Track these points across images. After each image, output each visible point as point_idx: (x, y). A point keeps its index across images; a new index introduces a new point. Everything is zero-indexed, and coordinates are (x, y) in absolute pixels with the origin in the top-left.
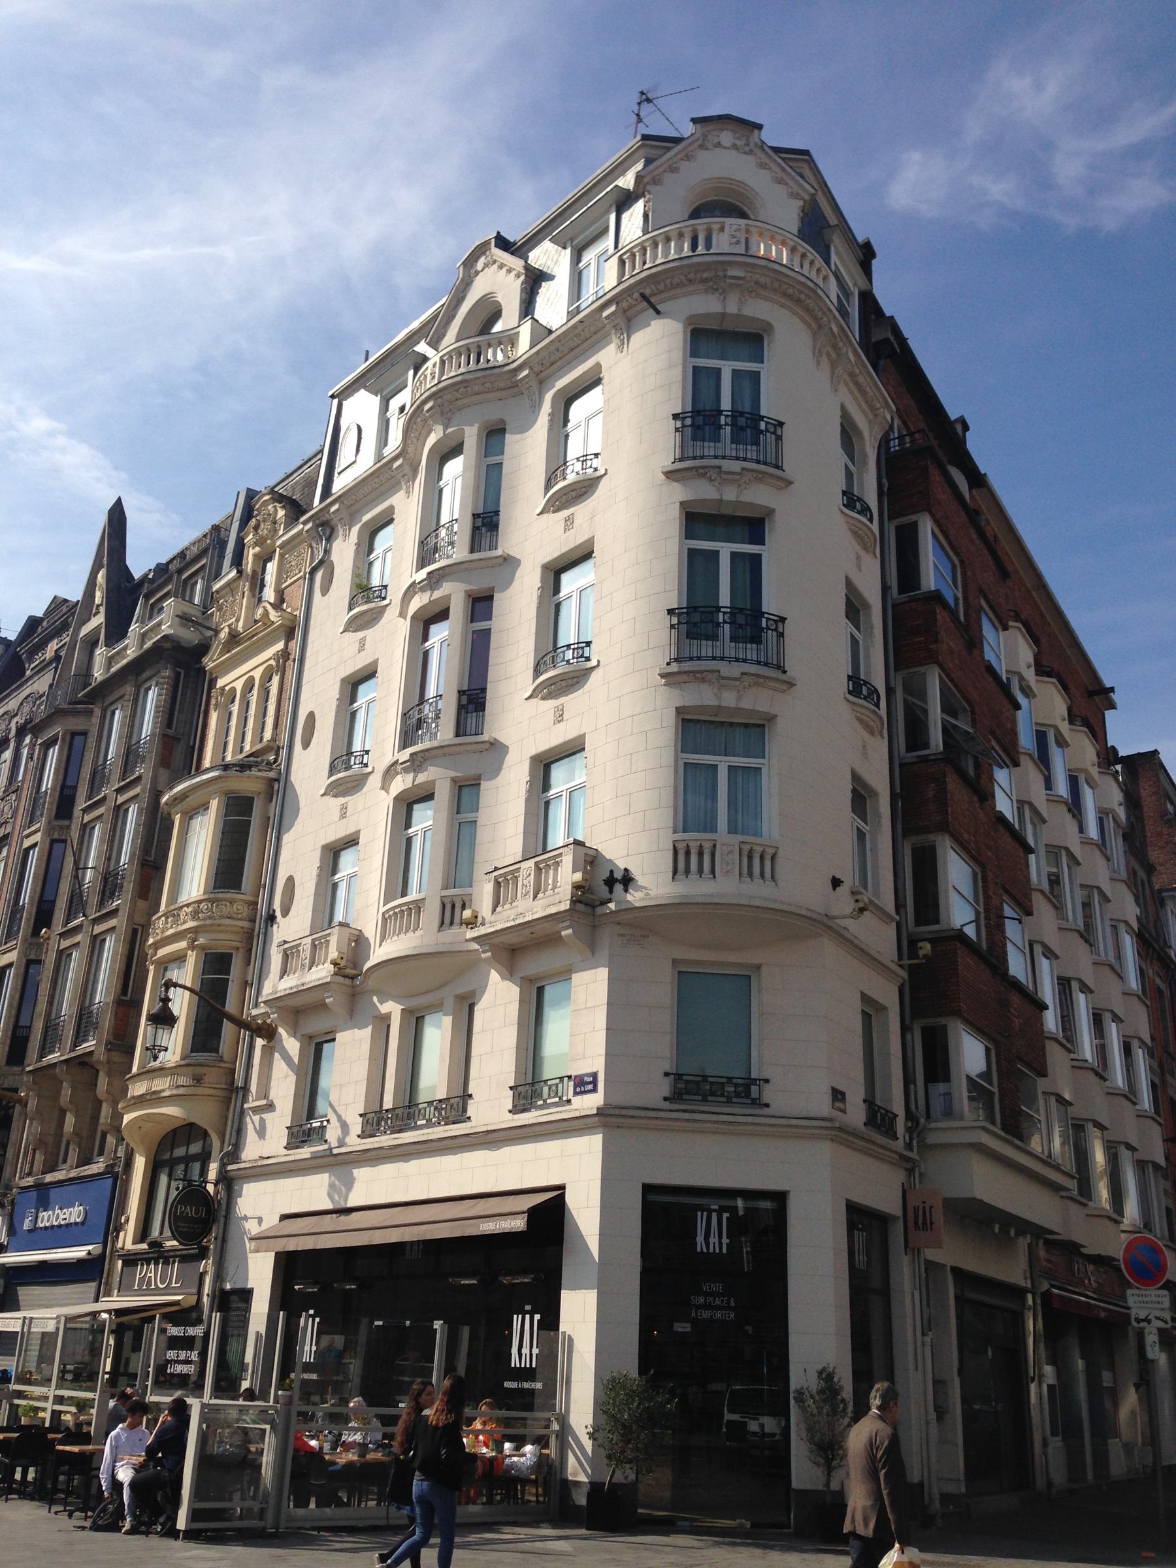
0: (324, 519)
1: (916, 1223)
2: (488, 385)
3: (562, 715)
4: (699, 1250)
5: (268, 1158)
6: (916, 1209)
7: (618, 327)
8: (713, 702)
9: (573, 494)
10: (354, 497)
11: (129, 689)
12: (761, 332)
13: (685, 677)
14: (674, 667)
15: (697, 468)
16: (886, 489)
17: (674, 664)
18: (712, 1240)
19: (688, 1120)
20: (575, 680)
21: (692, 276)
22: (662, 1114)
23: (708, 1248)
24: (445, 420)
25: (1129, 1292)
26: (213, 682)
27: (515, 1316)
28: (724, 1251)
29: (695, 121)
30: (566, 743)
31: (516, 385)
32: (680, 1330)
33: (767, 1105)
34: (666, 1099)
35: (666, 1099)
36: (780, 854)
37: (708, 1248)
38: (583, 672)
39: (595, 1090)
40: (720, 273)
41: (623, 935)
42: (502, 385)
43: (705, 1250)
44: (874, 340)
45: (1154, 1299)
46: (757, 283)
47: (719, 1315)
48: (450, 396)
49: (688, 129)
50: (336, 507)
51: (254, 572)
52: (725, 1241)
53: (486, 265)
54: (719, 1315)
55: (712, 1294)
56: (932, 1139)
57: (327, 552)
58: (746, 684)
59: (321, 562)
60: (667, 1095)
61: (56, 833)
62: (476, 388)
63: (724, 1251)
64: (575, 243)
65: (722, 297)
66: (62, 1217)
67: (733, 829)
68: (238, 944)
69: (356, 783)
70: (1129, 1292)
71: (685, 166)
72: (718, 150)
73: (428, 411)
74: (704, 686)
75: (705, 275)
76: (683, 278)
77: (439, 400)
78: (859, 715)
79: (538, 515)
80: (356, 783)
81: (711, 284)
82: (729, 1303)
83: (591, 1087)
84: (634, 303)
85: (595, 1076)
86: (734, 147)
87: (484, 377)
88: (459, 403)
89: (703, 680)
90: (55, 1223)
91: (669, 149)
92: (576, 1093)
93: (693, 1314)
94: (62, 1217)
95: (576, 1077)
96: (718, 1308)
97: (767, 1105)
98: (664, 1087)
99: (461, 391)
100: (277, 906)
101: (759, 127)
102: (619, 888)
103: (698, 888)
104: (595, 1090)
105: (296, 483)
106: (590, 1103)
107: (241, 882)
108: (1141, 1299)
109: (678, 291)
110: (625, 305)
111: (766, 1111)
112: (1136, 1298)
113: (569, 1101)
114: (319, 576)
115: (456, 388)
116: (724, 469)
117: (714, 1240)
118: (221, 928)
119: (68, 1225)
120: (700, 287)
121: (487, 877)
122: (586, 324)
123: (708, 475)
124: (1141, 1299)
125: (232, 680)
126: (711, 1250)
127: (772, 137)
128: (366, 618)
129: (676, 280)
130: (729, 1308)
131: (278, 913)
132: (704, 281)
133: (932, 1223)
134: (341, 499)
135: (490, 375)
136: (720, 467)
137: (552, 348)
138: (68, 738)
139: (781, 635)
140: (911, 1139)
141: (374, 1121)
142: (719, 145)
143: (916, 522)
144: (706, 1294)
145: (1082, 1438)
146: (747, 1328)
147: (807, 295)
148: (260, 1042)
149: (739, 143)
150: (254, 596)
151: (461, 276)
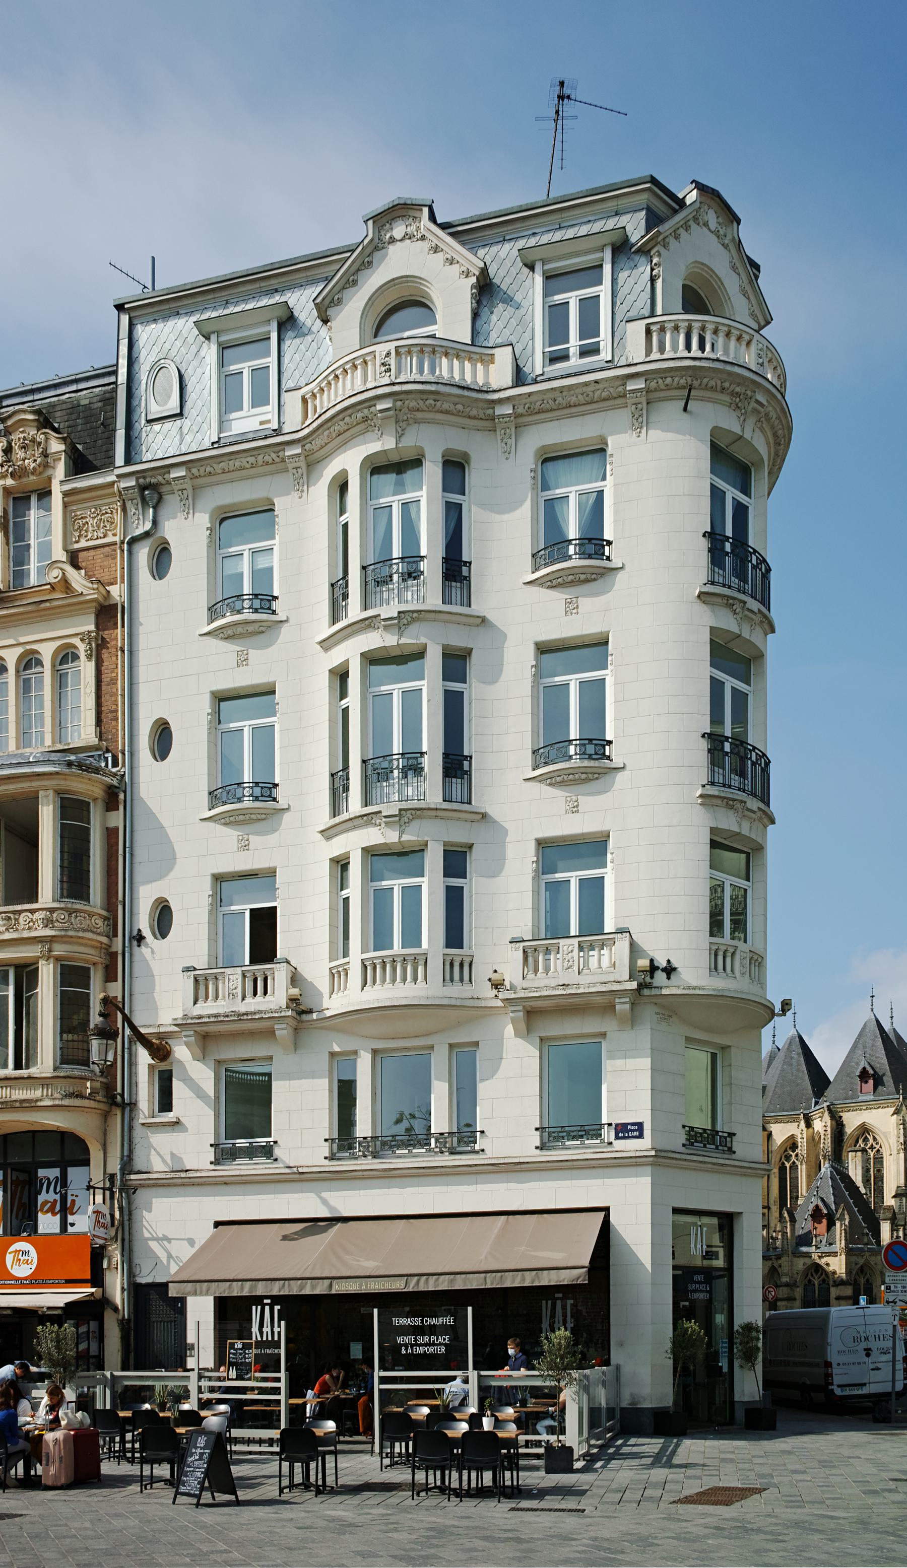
0: (153, 480)
2: (460, 407)
3: (577, 806)
7: (640, 406)
8: (735, 828)
9: (583, 577)
10: (209, 469)
12: (750, 465)
13: (719, 802)
14: (712, 791)
15: (730, 597)
17: (708, 787)
18: (265, 1330)
19: (701, 1162)
20: (596, 776)
21: (726, 385)
22: (684, 1157)
24: (399, 430)
27: (254, 1307)
30: (583, 834)
31: (492, 418)
33: (734, 1152)
38: (605, 770)
39: (641, 1136)
40: (749, 393)
42: (474, 412)
45: (901, 1278)
46: (767, 415)
48: (413, 404)
50: (181, 472)
53: (408, 237)
55: (700, 1283)
62: (446, 406)
64: (546, 267)
65: (742, 419)
68: (97, 959)
69: (264, 816)
73: (381, 411)
74: (731, 812)
75: (738, 389)
76: (719, 383)
77: (399, 403)
79: (524, 584)
80: (264, 816)
83: (637, 1134)
84: (663, 387)
85: (640, 1126)
87: (458, 396)
88: (419, 415)
89: (732, 807)
92: (617, 1137)
95: (617, 1125)
98: (682, 1138)
99: (428, 402)
102: (660, 977)
103: (719, 984)
104: (641, 1136)
106: (642, 1145)
107: (88, 894)
109: (708, 394)
110: (653, 385)
111: (734, 1156)
115: (425, 397)
116: (748, 605)
118: (80, 941)
120: (727, 398)
122: (601, 386)
126: (265, 1339)
128: (251, 628)
129: (712, 383)
132: (733, 394)
134: (190, 465)
135: (464, 396)
136: (745, 603)
137: (550, 395)
144: (696, 1283)
151: (370, 236)
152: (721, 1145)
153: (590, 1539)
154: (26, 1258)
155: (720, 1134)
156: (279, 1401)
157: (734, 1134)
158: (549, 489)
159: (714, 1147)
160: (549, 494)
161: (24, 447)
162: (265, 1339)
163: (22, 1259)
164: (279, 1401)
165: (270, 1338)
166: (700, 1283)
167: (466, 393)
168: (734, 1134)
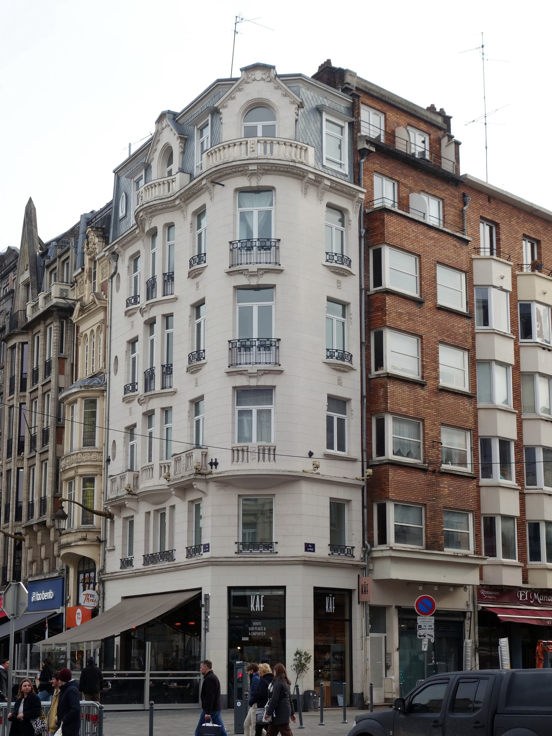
1: (362, 591)
4: (252, 610)
5: (115, 572)
6: (362, 585)
11: (41, 328)
16: (363, 235)
18: (257, 606)
23: (255, 610)
25: (418, 617)
26: (78, 327)
28: (262, 610)
29: (242, 70)
32: (244, 640)
34: (236, 553)
35: (236, 553)
36: (276, 449)
37: (255, 610)
41: (218, 486)
43: (254, 610)
44: (358, 149)
45: (428, 620)
47: (259, 634)
49: (237, 74)
51: (90, 269)
52: (262, 606)
54: (259, 634)
55: (258, 626)
56: (375, 555)
57: (116, 268)
58: (260, 374)
59: (115, 273)
60: (237, 551)
61: (22, 400)
63: (262, 610)
65: (249, 178)
66: (45, 596)
67: (259, 438)
70: (418, 617)
71: (238, 95)
72: (255, 82)
78: (333, 367)
81: (243, 172)
82: (263, 629)
86: (263, 79)
90: (43, 599)
91: (234, 84)
92: (204, 552)
93: (250, 634)
94: (45, 596)
96: (259, 631)
97: (277, 553)
100: (110, 454)
101: (274, 67)
105: (105, 217)
108: (423, 620)
112: (421, 620)
113: (202, 555)
114: (115, 279)
117: (258, 606)
119: (47, 600)
121: (172, 458)
123: (244, 273)
124: (423, 620)
125: (84, 328)
126: (257, 610)
127: (280, 71)
130: (263, 631)
131: (111, 458)
133: (367, 591)
138: (21, 346)
139: (278, 347)
140: (364, 556)
141: (149, 559)
142: (254, 80)
143: (381, 248)
144: (254, 626)
145: (156, 670)
146: (270, 638)
147: (291, 169)
148: (109, 520)
149: (264, 77)
150: (91, 282)
152: (348, 553)
153: (478, 708)
154: (93, 598)
155: (347, 547)
156: (26, 668)
157: (354, 547)
158: (152, 298)
159: (344, 555)
160: (243, 209)
161: (62, 242)
162: (257, 610)
163: (90, 599)
164: (26, 668)
165: (259, 610)
166: (258, 626)
167: (163, 201)
168: (354, 547)
